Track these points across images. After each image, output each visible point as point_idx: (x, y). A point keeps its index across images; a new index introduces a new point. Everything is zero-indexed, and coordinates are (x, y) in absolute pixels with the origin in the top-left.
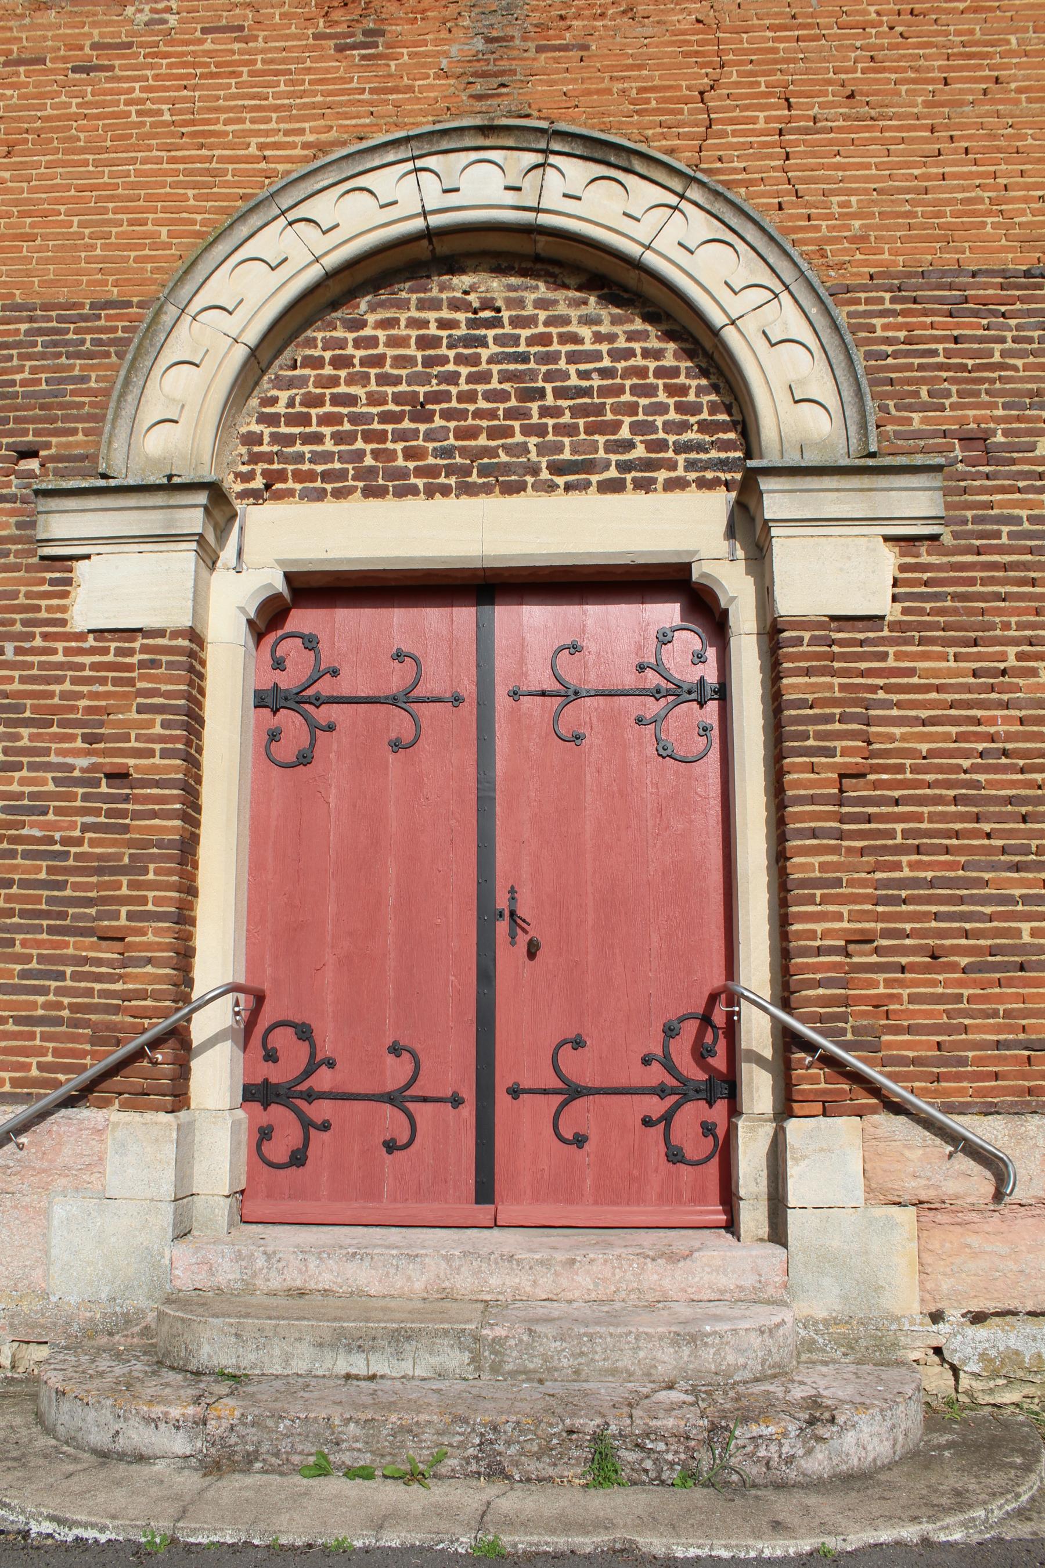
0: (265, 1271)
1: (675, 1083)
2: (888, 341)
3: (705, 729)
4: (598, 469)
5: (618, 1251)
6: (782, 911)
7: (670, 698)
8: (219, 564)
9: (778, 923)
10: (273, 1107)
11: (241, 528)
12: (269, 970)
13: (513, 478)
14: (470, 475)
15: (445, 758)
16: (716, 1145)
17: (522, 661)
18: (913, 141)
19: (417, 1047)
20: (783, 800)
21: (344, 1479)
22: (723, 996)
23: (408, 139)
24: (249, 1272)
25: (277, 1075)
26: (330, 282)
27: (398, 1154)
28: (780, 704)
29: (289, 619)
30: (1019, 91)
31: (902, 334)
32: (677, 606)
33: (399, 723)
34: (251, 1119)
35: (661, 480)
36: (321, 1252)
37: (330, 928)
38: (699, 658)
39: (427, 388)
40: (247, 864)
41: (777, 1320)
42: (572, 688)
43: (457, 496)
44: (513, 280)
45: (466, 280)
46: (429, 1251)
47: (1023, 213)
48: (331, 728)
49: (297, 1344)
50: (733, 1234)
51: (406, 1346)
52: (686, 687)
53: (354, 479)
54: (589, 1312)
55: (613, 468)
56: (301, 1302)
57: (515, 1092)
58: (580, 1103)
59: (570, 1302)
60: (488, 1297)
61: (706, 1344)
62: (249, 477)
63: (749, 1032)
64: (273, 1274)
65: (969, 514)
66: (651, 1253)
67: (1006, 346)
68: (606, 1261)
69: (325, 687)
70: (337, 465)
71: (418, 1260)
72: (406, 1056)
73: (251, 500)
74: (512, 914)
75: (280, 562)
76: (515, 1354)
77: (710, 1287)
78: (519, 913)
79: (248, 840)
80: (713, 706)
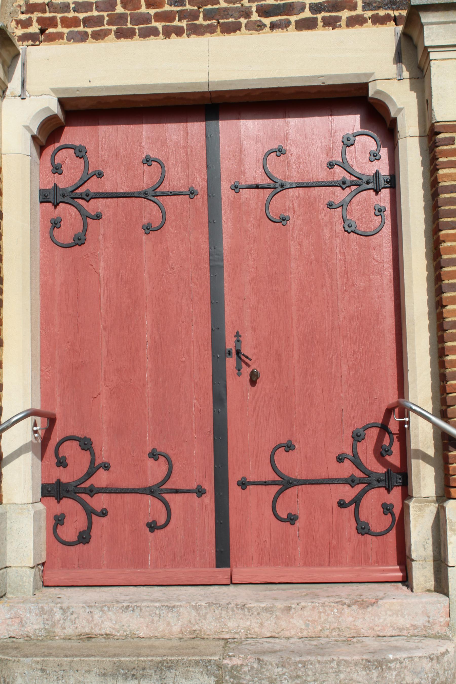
0: (62, 622)
1: (362, 475)
3: (380, 211)
4: (296, 11)
5: (323, 600)
6: (440, 346)
7: (353, 188)
8: (8, 93)
9: (437, 355)
10: (65, 501)
11: (24, 65)
12: (58, 399)
13: (231, 20)
14: (197, 19)
15: (185, 238)
16: (393, 521)
17: (240, 162)
19: (170, 453)
20: (439, 262)
21: (132, 681)
22: (397, 410)
24: (50, 623)
25: (67, 476)
27: (158, 532)
28: (437, 190)
29: (64, 135)
32: (358, 117)
33: (149, 212)
34: (48, 510)
35: (344, 18)
36: (103, 606)
37: (102, 366)
38: (375, 157)
40: (39, 320)
41: (442, 650)
42: (279, 182)
43: (188, 36)
46: (183, 603)
48: (98, 217)
49: (87, 675)
50: (408, 586)
51: (168, 673)
52: (365, 179)
53: (109, 24)
54: (302, 645)
55: (307, 10)
56: (89, 644)
57: (243, 484)
58: (291, 492)
59: (288, 638)
60: (227, 636)
61: (390, 668)
62: (26, 24)
63: (417, 436)
64: (68, 623)
66: (347, 601)
68: (314, 608)
69: (93, 186)
70: (95, 13)
71: (175, 610)
72: (162, 459)
73: (30, 42)
74: (238, 352)
75: (55, 91)
76: (248, 677)
77: (391, 626)
78: (243, 352)
79: (39, 303)
80: (385, 193)
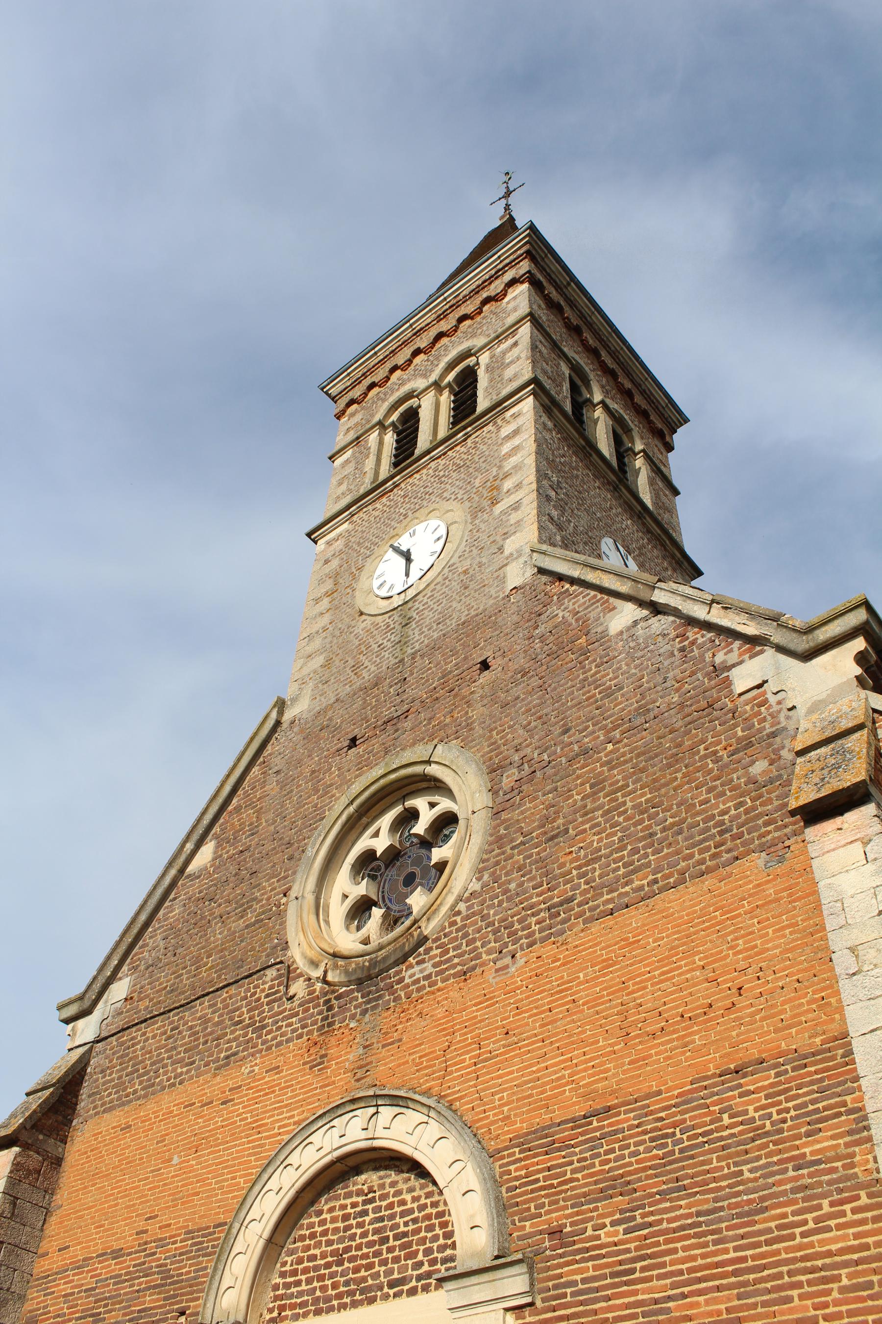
2: (517, 1178)
18: (534, 1050)
23: (324, 1114)
26: (302, 1194)
30: (583, 1004)
31: (523, 1172)
39: (344, 1245)
44: (382, 1173)
45: (363, 1177)
47: (584, 1078)
65: (550, 1284)
67: (573, 1166)
